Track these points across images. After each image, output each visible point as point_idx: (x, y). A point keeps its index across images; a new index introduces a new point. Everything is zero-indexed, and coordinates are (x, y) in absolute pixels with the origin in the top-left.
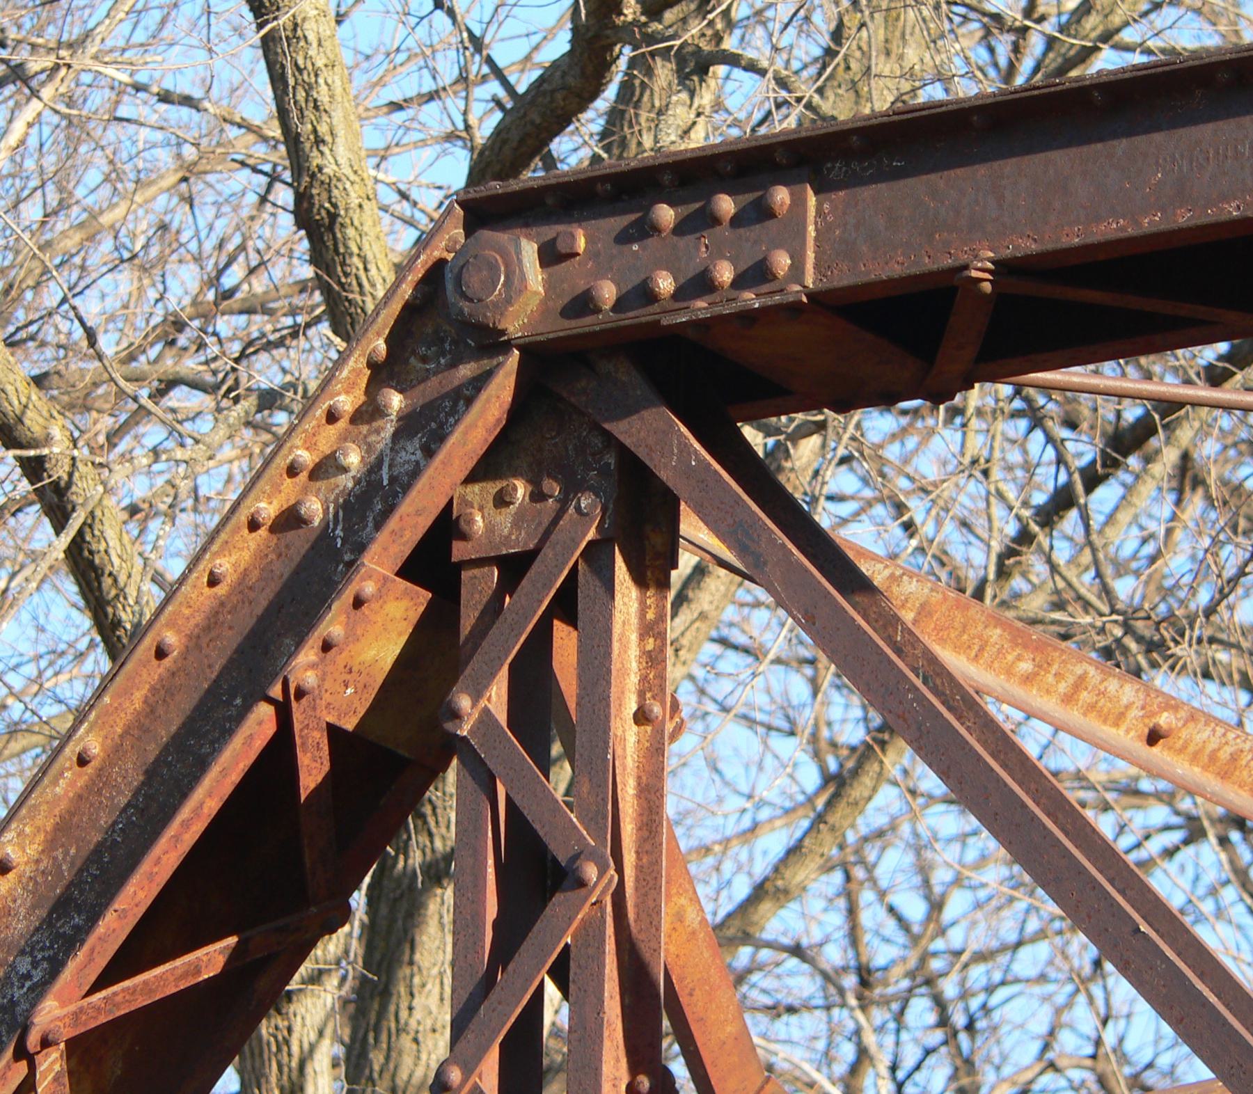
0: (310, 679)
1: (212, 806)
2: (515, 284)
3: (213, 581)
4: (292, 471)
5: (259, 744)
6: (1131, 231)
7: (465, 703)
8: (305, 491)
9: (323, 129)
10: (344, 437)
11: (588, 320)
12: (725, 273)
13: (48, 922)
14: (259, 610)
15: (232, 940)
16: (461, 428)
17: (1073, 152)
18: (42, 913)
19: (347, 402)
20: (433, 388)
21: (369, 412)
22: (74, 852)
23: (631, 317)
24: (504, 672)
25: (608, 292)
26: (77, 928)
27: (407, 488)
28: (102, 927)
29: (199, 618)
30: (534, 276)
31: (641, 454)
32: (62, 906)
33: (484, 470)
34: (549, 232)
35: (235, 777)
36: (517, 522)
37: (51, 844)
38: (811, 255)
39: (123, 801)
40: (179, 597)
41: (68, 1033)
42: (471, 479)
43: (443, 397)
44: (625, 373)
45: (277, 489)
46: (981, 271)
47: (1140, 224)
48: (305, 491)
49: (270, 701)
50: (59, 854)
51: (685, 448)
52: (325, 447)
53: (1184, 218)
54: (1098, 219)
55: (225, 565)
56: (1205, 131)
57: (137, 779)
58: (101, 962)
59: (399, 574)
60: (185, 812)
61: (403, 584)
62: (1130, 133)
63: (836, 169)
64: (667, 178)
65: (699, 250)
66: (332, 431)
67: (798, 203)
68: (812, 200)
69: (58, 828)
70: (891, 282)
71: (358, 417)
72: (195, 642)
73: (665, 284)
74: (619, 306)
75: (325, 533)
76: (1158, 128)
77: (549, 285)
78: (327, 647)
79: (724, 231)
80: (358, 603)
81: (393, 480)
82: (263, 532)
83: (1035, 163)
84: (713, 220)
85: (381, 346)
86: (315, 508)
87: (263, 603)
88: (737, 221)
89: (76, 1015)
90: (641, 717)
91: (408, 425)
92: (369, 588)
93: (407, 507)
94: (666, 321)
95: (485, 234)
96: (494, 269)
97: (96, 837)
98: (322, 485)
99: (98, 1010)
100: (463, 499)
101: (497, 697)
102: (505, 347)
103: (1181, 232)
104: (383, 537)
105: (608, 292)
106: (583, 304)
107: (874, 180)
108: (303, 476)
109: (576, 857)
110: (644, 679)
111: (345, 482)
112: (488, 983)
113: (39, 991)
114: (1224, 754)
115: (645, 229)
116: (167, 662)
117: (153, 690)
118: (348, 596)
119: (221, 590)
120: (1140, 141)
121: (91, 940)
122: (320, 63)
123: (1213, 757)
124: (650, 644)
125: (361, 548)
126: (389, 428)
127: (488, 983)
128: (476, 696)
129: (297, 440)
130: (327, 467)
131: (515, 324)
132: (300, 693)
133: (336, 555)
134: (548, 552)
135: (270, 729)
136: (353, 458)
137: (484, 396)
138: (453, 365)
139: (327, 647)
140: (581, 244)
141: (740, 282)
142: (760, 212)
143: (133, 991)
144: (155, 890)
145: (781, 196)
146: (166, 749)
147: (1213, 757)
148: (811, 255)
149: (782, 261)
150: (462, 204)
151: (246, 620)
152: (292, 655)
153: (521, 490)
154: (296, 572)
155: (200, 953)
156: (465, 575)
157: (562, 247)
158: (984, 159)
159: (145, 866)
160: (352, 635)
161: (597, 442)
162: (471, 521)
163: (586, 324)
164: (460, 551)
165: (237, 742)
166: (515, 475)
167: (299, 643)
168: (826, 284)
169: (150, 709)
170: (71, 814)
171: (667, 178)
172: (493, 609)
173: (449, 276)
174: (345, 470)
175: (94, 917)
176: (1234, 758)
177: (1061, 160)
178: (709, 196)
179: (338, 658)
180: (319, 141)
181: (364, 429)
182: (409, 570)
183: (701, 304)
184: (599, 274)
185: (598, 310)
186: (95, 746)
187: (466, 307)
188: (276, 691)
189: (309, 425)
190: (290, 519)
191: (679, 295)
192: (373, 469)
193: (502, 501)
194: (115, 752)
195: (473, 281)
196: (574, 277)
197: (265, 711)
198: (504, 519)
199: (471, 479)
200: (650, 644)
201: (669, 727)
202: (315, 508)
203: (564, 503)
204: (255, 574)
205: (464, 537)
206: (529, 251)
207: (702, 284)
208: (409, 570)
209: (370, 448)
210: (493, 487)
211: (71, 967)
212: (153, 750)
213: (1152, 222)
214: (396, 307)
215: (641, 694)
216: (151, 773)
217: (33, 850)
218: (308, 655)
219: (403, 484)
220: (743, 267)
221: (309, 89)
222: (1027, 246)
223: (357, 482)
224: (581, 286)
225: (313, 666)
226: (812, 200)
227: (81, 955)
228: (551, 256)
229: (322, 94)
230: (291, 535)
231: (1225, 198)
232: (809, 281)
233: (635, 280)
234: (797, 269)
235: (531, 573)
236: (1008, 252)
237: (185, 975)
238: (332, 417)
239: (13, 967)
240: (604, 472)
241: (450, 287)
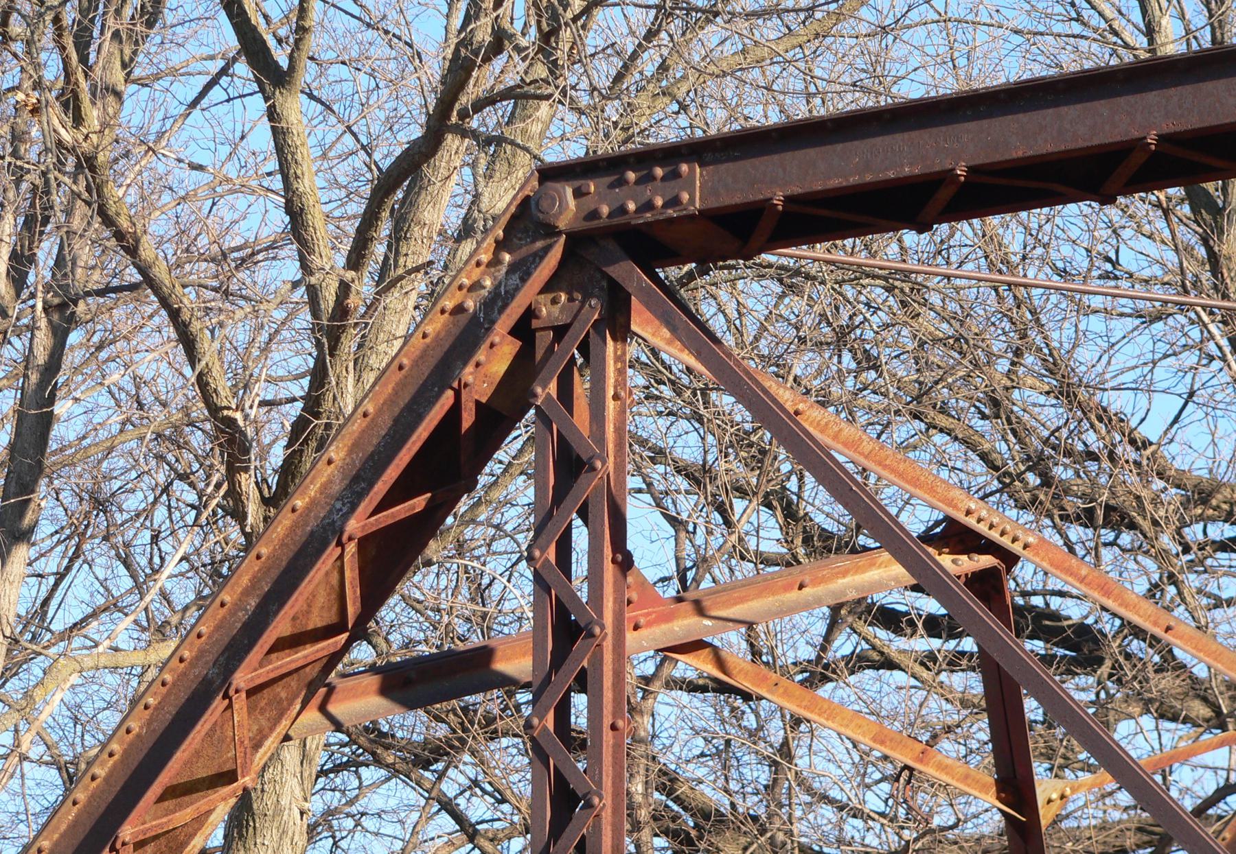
0: (470, 379)
1: (425, 435)
2: (563, 206)
3: (425, 336)
4: (460, 288)
5: (446, 408)
6: (844, 184)
7: (539, 390)
8: (466, 297)
9: (299, 172)
10: (483, 274)
11: (596, 222)
12: (659, 202)
13: (349, 486)
14: (445, 349)
15: (429, 495)
16: (539, 269)
17: (817, 149)
18: (346, 482)
19: (485, 258)
20: (524, 252)
21: (495, 262)
22: (360, 456)
23: (617, 221)
24: (555, 379)
25: (605, 210)
26: (363, 489)
27: (513, 297)
28: (376, 488)
29: (418, 353)
30: (571, 203)
31: (620, 280)
32: (356, 479)
33: (547, 288)
34: (577, 183)
35: (436, 422)
36: (561, 312)
37: (350, 452)
38: (698, 194)
39: (383, 433)
40: (410, 343)
41: (359, 535)
42: (541, 292)
43: (529, 256)
44: (612, 245)
45: (453, 295)
46: (778, 200)
47: (848, 180)
48: (466, 297)
49: (453, 389)
50: (354, 456)
51: (640, 278)
52: (475, 277)
53: (869, 178)
54: (830, 179)
55: (430, 329)
56: (878, 140)
57: (389, 423)
58: (375, 503)
59: (510, 333)
60: (414, 438)
61: (510, 338)
62: (843, 142)
63: (709, 156)
64: (632, 160)
65: (647, 192)
66: (478, 271)
67: (692, 171)
68: (698, 170)
69: (353, 445)
70: (736, 205)
71: (489, 265)
72: (416, 363)
73: (631, 206)
74: (610, 216)
75: (475, 315)
76: (855, 139)
77: (577, 206)
78: (478, 365)
79: (658, 183)
80: (492, 346)
81: (506, 292)
82: (446, 315)
83: (800, 154)
84: (626, 182)
85: (501, 233)
86: (470, 304)
87: (447, 346)
88: (664, 179)
89: (363, 527)
90: (616, 397)
91: (513, 268)
92: (497, 339)
93: (514, 304)
94: (633, 222)
95: (549, 184)
96: (554, 199)
97: (371, 449)
98: (473, 294)
99: (372, 524)
100: (537, 301)
101: (553, 388)
102: (560, 233)
103: (869, 184)
104: (504, 317)
105: (605, 210)
106: (594, 215)
107: (727, 161)
108: (465, 290)
109: (591, 458)
110: (616, 381)
111: (484, 293)
112: (549, 516)
113: (346, 517)
114: (823, 423)
115: (622, 182)
116: (403, 372)
117: (397, 384)
118: (488, 343)
119: (428, 340)
120: (848, 144)
121: (371, 494)
122: (298, 143)
123: (818, 424)
124: (619, 365)
125: (493, 322)
126: (504, 269)
127: (549, 516)
128: (544, 387)
129: (463, 274)
130: (476, 286)
131: (562, 224)
132: (466, 385)
133: (481, 325)
134: (576, 324)
135: (451, 401)
136: (488, 283)
137: (550, 255)
138: (533, 241)
139: (478, 365)
140: (592, 189)
141: (666, 205)
142: (676, 175)
143: (387, 517)
144: (399, 472)
145: (684, 168)
146: (402, 411)
147: (818, 424)
148: (698, 194)
149: (685, 197)
150: (538, 171)
151: (438, 354)
152: (462, 369)
153: (563, 297)
154: (462, 333)
155: (415, 500)
156: (537, 334)
157: (584, 190)
158: (776, 153)
159: (396, 461)
160: (488, 361)
161: (598, 276)
162: (541, 311)
163: (594, 224)
164: (535, 324)
165: (437, 407)
166: (561, 290)
167: (465, 364)
168: (705, 207)
169: (396, 392)
170: (359, 438)
171: (578, 170)
172: (550, 351)
173: (533, 203)
174: (484, 288)
175: (371, 485)
176: (827, 424)
177: (812, 153)
178: (677, 164)
179: (482, 370)
180: (297, 177)
181: (493, 270)
182: (514, 332)
183: (648, 215)
184: (602, 201)
185: (600, 218)
186: (371, 410)
187: (541, 216)
188: (455, 385)
189: (469, 268)
190: (459, 309)
191: (637, 211)
192: (497, 287)
193: (554, 301)
194: (379, 412)
195: (544, 204)
196: (589, 204)
197: (449, 394)
198: (556, 310)
199: (541, 292)
200: (619, 365)
201: (628, 402)
202: (470, 304)
203: (583, 303)
204: (443, 334)
205: (537, 317)
206: (569, 191)
207: (648, 206)
208: (514, 332)
209: (495, 278)
210: (551, 296)
211: (363, 505)
212: (397, 411)
213: (854, 180)
214: (508, 216)
215: (615, 387)
216: (396, 421)
217: (342, 454)
218: (470, 368)
219: (511, 295)
220: (667, 199)
221: (293, 154)
222: (797, 190)
223: (490, 293)
224: (593, 207)
225: (471, 374)
226: (698, 170)
227: (367, 500)
228: (578, 194)
229: (299, 157)
230: (459, 317)
231: (887, 169)
232: (697, 206)
233: (617, 205)
234: (692, 200)
235: (569, 334)
236: (789, 193)
237: (409, 510)
238: (478, 264)
239: (333, 506)
240: (601, 289)
241: (533, 206)
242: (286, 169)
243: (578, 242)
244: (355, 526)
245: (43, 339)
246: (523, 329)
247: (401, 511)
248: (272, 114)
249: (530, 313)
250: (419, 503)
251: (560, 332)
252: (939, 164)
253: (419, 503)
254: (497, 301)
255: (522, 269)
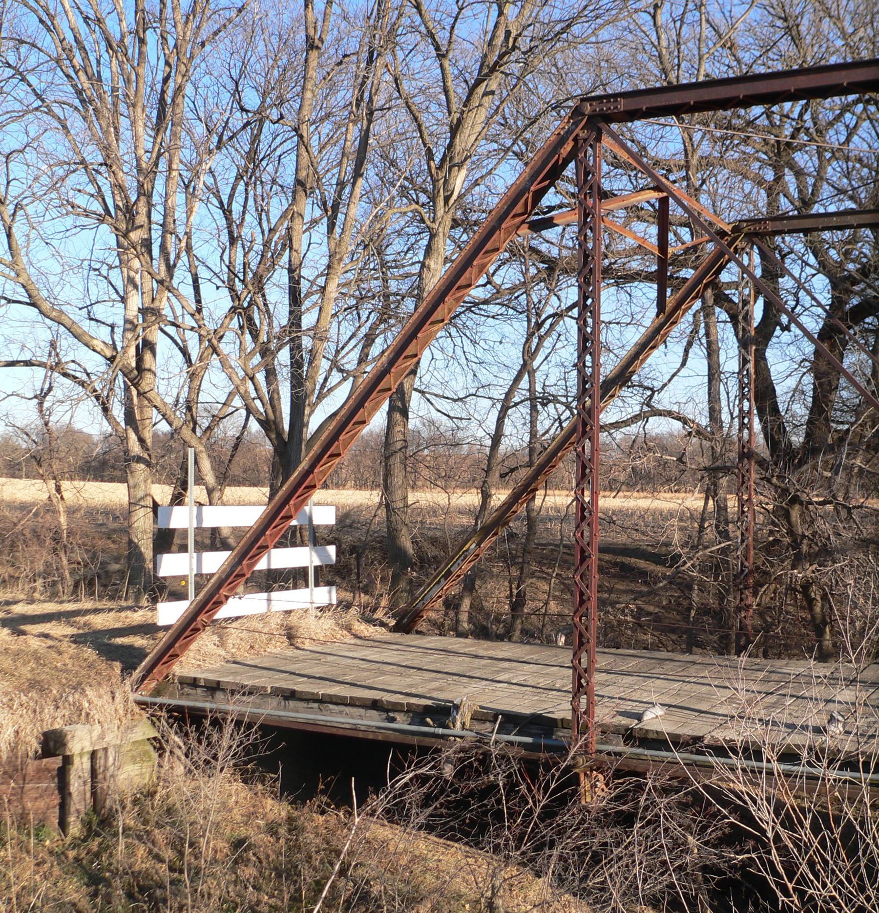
242: (444, 80)
243: (591, 117)
244: (532, 188)
245: (365, 122)
246: (575, 140)
247: (542, 185)
248: (441, 66)
249: (577, 135)
250: (547, 182)
251: (585, 140)
252: (686, 100)
253: (547, 182)
254: (569, 132)
255: (576, 124)
